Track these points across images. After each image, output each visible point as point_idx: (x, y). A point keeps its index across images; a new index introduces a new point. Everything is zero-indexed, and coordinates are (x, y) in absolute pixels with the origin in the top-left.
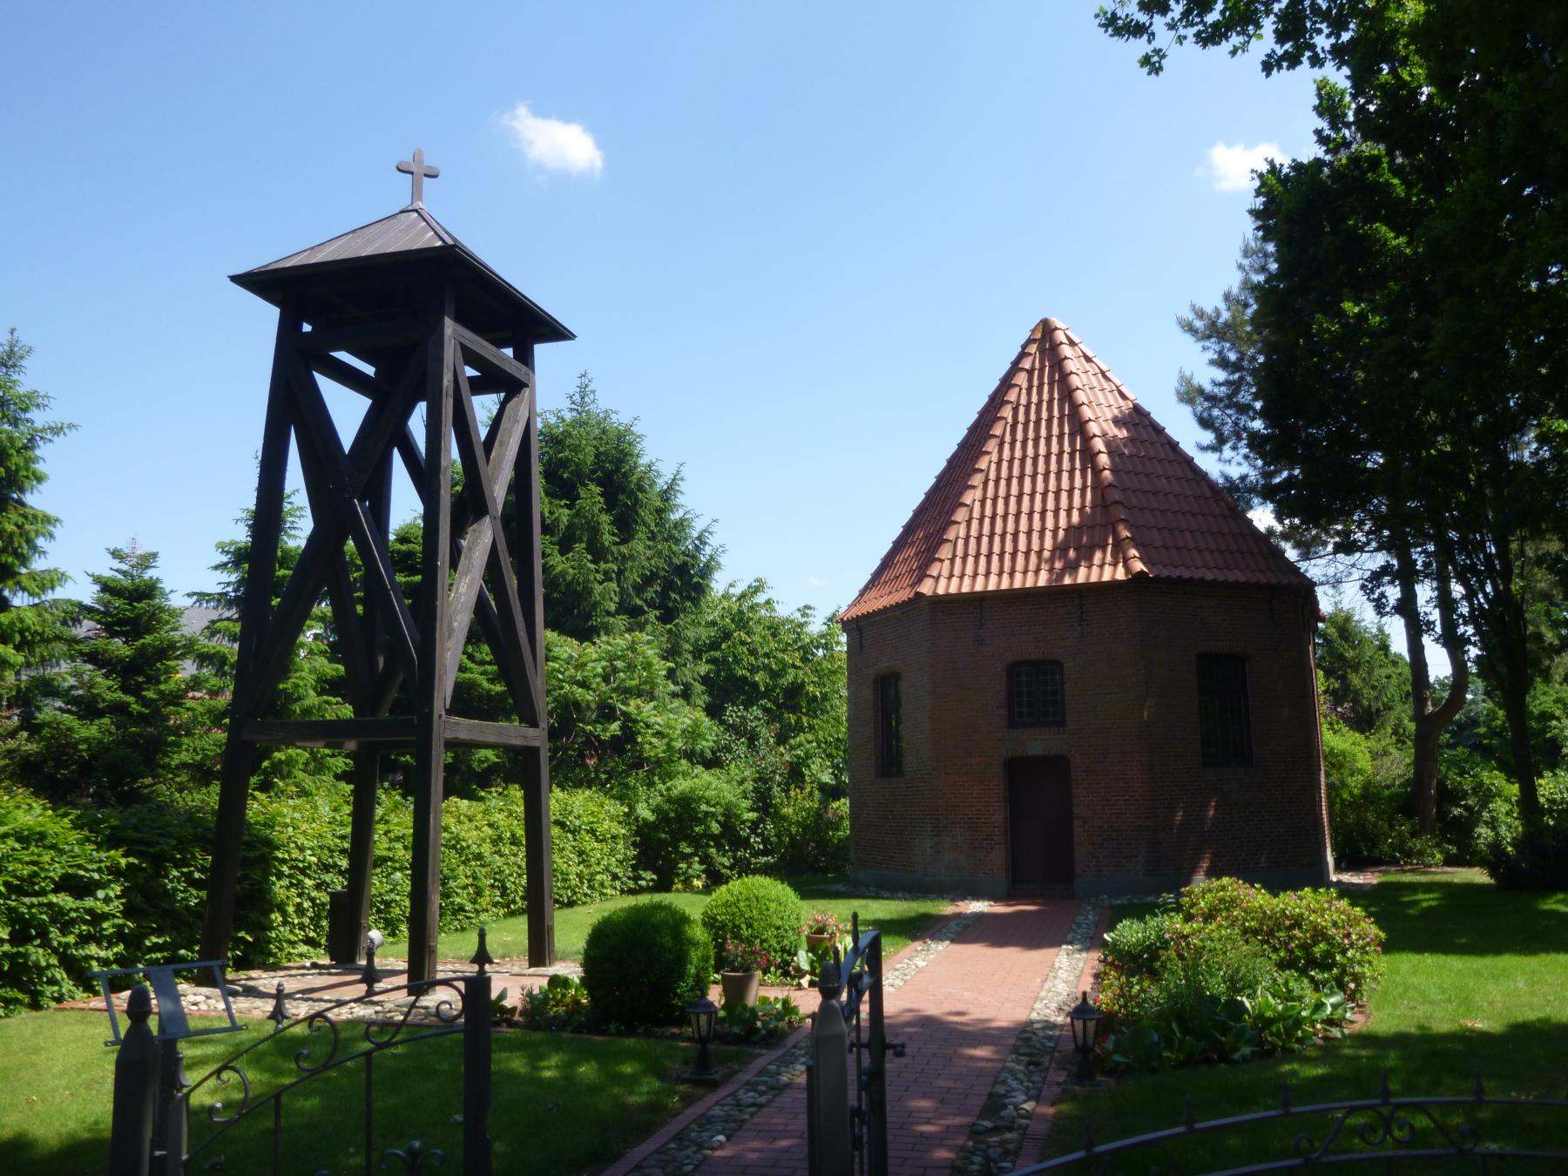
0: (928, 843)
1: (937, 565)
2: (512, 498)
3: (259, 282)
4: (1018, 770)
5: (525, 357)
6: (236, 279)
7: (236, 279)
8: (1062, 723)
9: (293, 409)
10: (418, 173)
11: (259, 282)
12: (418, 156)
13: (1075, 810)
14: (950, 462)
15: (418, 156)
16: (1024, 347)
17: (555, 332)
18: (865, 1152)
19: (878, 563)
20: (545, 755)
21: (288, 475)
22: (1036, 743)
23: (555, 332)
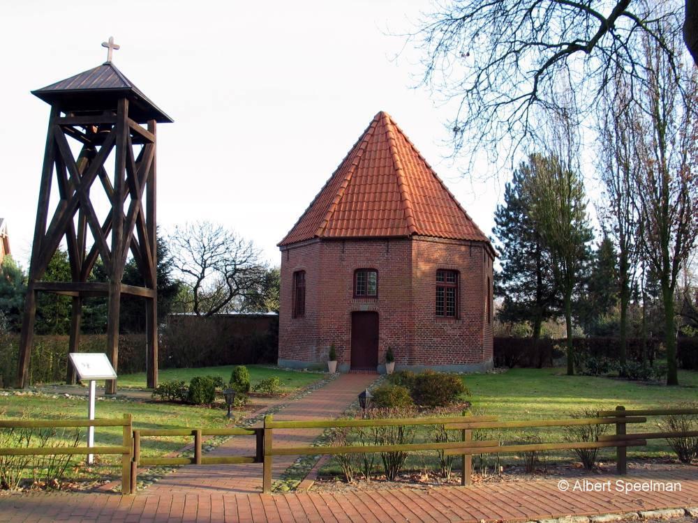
0: (315, 348)
1: (325, 223)
2: (88, 204)
3: (43, 94)
4: (355, 315)
5: (152, 129)
6: (34, 93)
7: (34, 93)
8: (355, 297)
9: (55, 153)
10: (110, 46)
11: (43, 94)
12: (111, 40)
13: (380, 336)
14: (334, 175)
15: (111, 40)
16: (371, 124)
17: (164, 119)
18: (47, 420)
19: (298, 220)
20: (155, 300)
21: (110, 154)
22: (364, 306)
23: (164, 119)
